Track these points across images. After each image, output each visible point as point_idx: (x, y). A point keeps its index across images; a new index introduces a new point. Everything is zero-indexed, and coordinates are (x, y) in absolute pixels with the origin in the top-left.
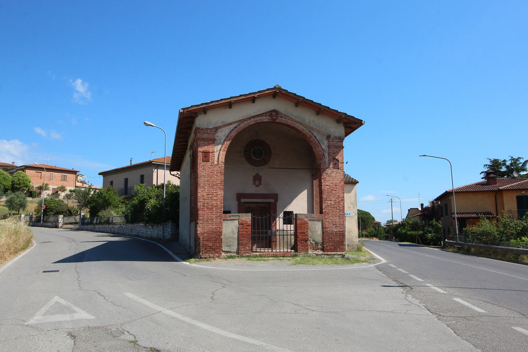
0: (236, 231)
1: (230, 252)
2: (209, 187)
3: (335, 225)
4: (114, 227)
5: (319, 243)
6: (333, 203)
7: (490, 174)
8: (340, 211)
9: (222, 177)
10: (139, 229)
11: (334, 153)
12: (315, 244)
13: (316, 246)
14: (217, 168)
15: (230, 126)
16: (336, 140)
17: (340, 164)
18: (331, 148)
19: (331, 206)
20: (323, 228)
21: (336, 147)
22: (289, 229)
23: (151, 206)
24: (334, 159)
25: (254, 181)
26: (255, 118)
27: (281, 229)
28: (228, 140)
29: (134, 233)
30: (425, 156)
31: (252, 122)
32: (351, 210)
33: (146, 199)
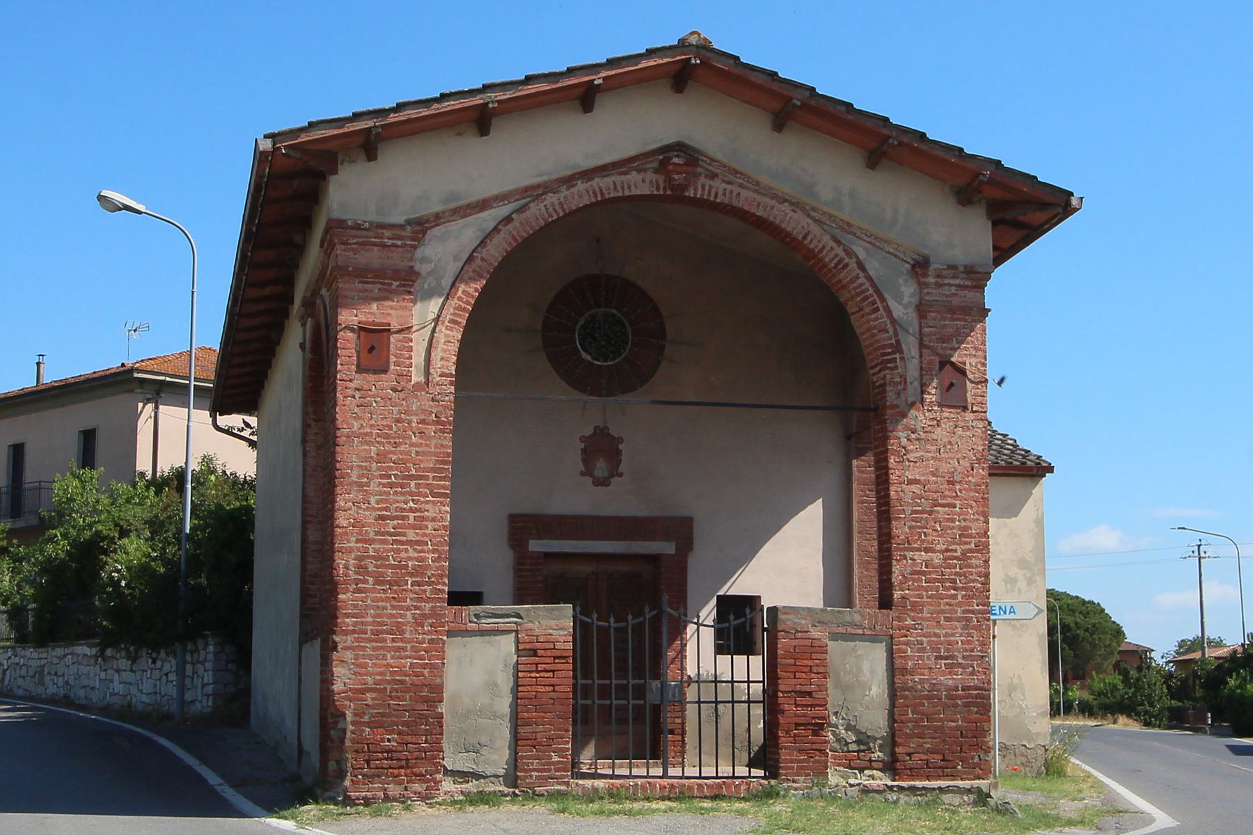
1: (477, 776)
2: (384, 485)
3: (946, 658)
5: (876, 739)
6: (937, 559)
9: (445, 443)
11: (944, 340)
12: (858, 742)
13: (863, 751)
14: (421, 402)
15: (481, 215)
16: (951, 282)
19: (930, 573)
20: (892, 670)
23: (129, 569)
24: (945, 363)
25: (585, 461)
28: (470, 278)
29: (52, 690)
31: (581, 197)
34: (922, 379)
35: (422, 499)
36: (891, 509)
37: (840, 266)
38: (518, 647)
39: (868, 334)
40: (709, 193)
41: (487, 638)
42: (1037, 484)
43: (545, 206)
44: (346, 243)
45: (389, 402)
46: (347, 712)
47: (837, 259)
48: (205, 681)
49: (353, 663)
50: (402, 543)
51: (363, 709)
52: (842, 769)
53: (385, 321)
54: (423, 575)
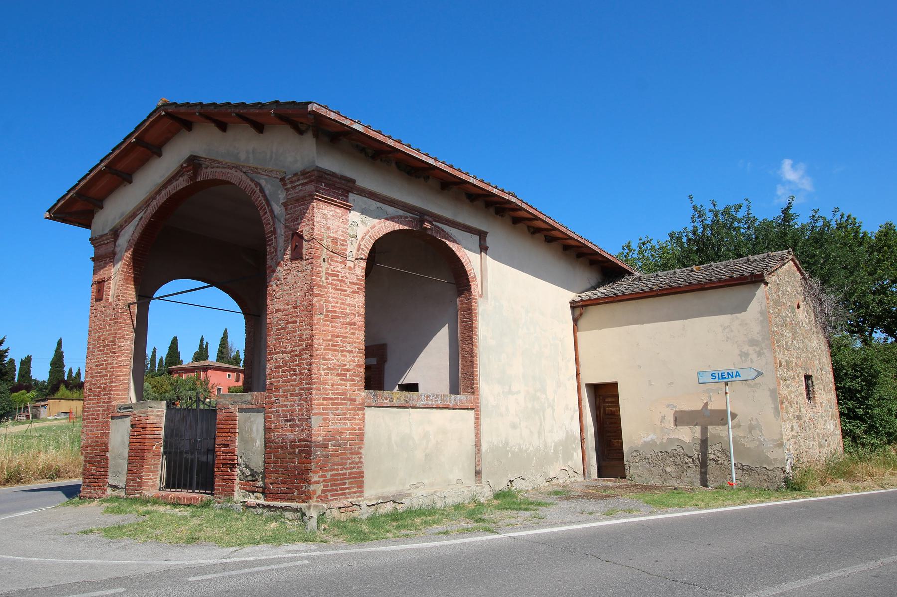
3: (290, 421)
5: (259, 474)
18: (290, 206)
20: (267, 430)
26: (167, 187)
31: (163, 198)
42: (760, 287)
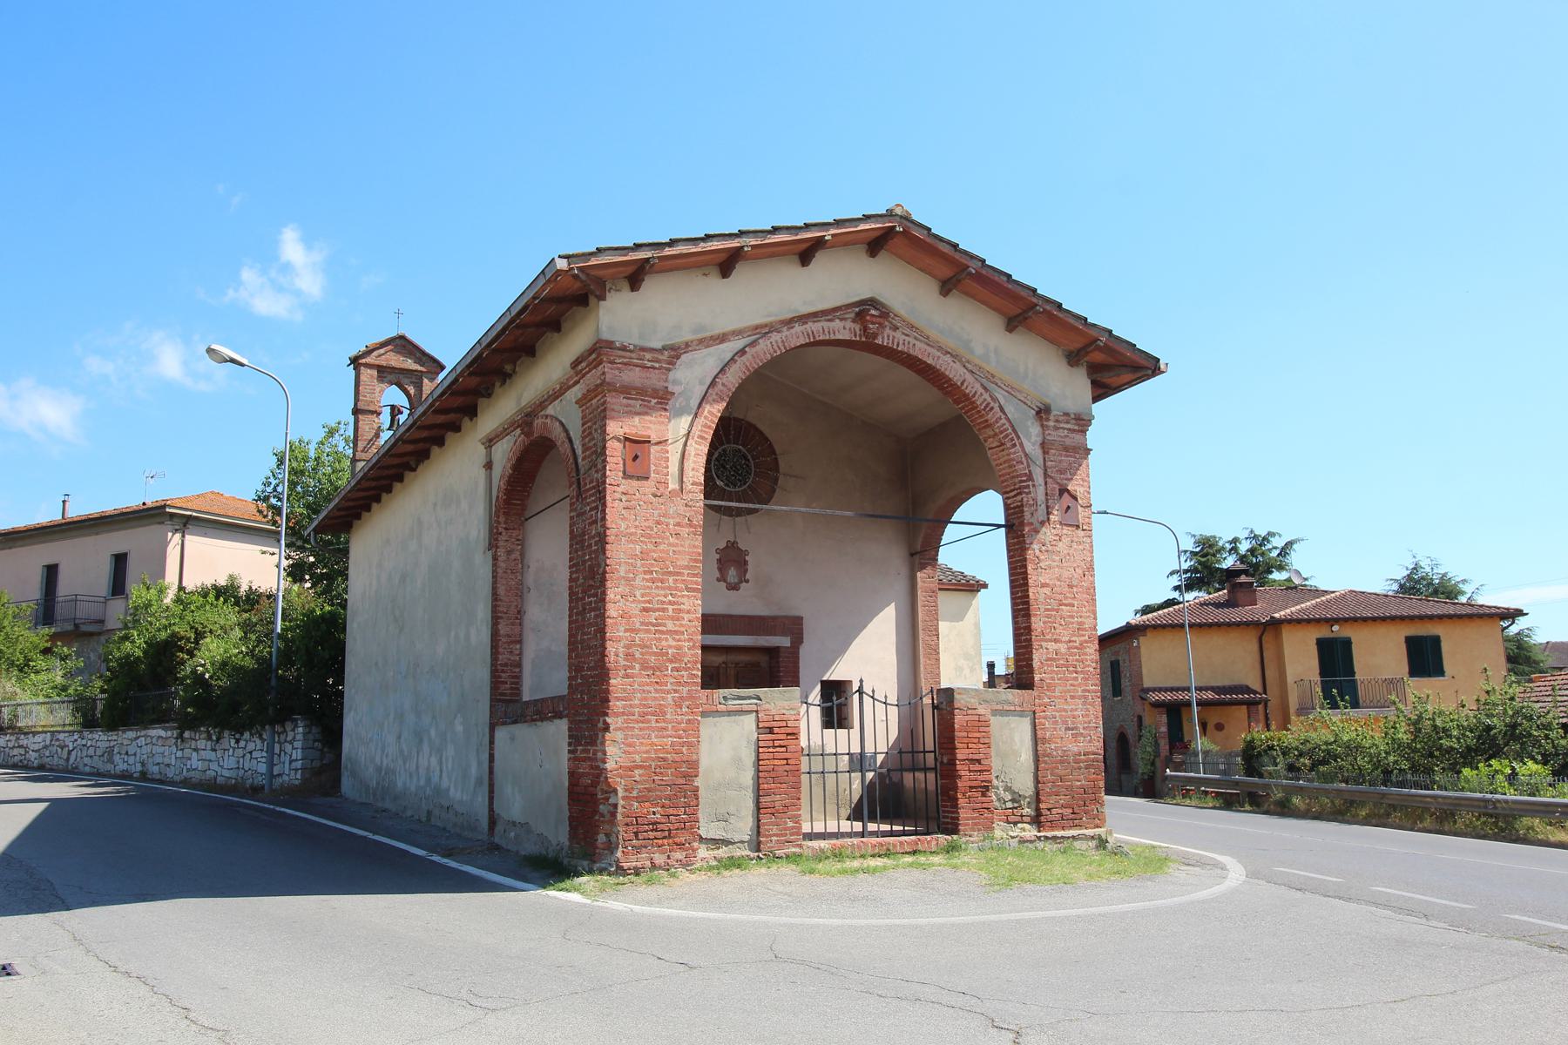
0: (749, 759)
1: (727, 842)
2: (647, 581)
4: (25, 742)
5: (1026, 797)
6: (1063, 648)
7: (1239, 576)
8: (1087, 679)
9: (697, 543)
10: (148, 749)
11: (1061, 472)
12: (1013, 800)
13: (1016, 808)
14: (676, 507)
15: (721, 346)
17: (1080, 509)
19: (1059, 659)
21: (1066, 449)
22: (830, 749)
23: (213, 664)
24: (1063, 491)
25: (720, 569)
26: (807, 323)
27: (828, 751)
28: (714, 400)
29: (122, 767)
30: (1105, 512)
32: (965, 678)
33: (182, 638)
34: (1047, 503)
35: (679, 594)
36: (1031, 607)
37: (988, 409)
38: (758, 725)
39: (1007, 465)
40: (893, 343)
41: (733, 717)
43: (771, 343)
44: (612, 362)
45: (650, 505)
46: (619, 788)
47: (986, 403)
48: (294, 757)
49: (623, 743)
50: (662, 632)
51: (632, 784)
52: (1002, 823)
53: (644, 433)
54: (681, 661)
